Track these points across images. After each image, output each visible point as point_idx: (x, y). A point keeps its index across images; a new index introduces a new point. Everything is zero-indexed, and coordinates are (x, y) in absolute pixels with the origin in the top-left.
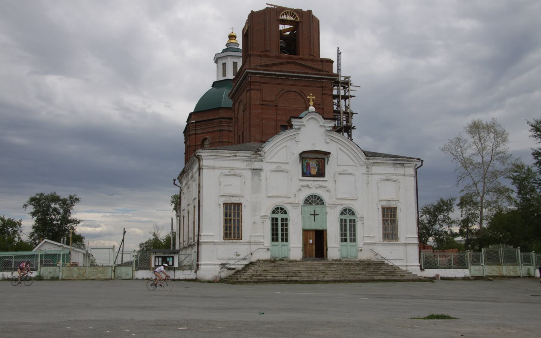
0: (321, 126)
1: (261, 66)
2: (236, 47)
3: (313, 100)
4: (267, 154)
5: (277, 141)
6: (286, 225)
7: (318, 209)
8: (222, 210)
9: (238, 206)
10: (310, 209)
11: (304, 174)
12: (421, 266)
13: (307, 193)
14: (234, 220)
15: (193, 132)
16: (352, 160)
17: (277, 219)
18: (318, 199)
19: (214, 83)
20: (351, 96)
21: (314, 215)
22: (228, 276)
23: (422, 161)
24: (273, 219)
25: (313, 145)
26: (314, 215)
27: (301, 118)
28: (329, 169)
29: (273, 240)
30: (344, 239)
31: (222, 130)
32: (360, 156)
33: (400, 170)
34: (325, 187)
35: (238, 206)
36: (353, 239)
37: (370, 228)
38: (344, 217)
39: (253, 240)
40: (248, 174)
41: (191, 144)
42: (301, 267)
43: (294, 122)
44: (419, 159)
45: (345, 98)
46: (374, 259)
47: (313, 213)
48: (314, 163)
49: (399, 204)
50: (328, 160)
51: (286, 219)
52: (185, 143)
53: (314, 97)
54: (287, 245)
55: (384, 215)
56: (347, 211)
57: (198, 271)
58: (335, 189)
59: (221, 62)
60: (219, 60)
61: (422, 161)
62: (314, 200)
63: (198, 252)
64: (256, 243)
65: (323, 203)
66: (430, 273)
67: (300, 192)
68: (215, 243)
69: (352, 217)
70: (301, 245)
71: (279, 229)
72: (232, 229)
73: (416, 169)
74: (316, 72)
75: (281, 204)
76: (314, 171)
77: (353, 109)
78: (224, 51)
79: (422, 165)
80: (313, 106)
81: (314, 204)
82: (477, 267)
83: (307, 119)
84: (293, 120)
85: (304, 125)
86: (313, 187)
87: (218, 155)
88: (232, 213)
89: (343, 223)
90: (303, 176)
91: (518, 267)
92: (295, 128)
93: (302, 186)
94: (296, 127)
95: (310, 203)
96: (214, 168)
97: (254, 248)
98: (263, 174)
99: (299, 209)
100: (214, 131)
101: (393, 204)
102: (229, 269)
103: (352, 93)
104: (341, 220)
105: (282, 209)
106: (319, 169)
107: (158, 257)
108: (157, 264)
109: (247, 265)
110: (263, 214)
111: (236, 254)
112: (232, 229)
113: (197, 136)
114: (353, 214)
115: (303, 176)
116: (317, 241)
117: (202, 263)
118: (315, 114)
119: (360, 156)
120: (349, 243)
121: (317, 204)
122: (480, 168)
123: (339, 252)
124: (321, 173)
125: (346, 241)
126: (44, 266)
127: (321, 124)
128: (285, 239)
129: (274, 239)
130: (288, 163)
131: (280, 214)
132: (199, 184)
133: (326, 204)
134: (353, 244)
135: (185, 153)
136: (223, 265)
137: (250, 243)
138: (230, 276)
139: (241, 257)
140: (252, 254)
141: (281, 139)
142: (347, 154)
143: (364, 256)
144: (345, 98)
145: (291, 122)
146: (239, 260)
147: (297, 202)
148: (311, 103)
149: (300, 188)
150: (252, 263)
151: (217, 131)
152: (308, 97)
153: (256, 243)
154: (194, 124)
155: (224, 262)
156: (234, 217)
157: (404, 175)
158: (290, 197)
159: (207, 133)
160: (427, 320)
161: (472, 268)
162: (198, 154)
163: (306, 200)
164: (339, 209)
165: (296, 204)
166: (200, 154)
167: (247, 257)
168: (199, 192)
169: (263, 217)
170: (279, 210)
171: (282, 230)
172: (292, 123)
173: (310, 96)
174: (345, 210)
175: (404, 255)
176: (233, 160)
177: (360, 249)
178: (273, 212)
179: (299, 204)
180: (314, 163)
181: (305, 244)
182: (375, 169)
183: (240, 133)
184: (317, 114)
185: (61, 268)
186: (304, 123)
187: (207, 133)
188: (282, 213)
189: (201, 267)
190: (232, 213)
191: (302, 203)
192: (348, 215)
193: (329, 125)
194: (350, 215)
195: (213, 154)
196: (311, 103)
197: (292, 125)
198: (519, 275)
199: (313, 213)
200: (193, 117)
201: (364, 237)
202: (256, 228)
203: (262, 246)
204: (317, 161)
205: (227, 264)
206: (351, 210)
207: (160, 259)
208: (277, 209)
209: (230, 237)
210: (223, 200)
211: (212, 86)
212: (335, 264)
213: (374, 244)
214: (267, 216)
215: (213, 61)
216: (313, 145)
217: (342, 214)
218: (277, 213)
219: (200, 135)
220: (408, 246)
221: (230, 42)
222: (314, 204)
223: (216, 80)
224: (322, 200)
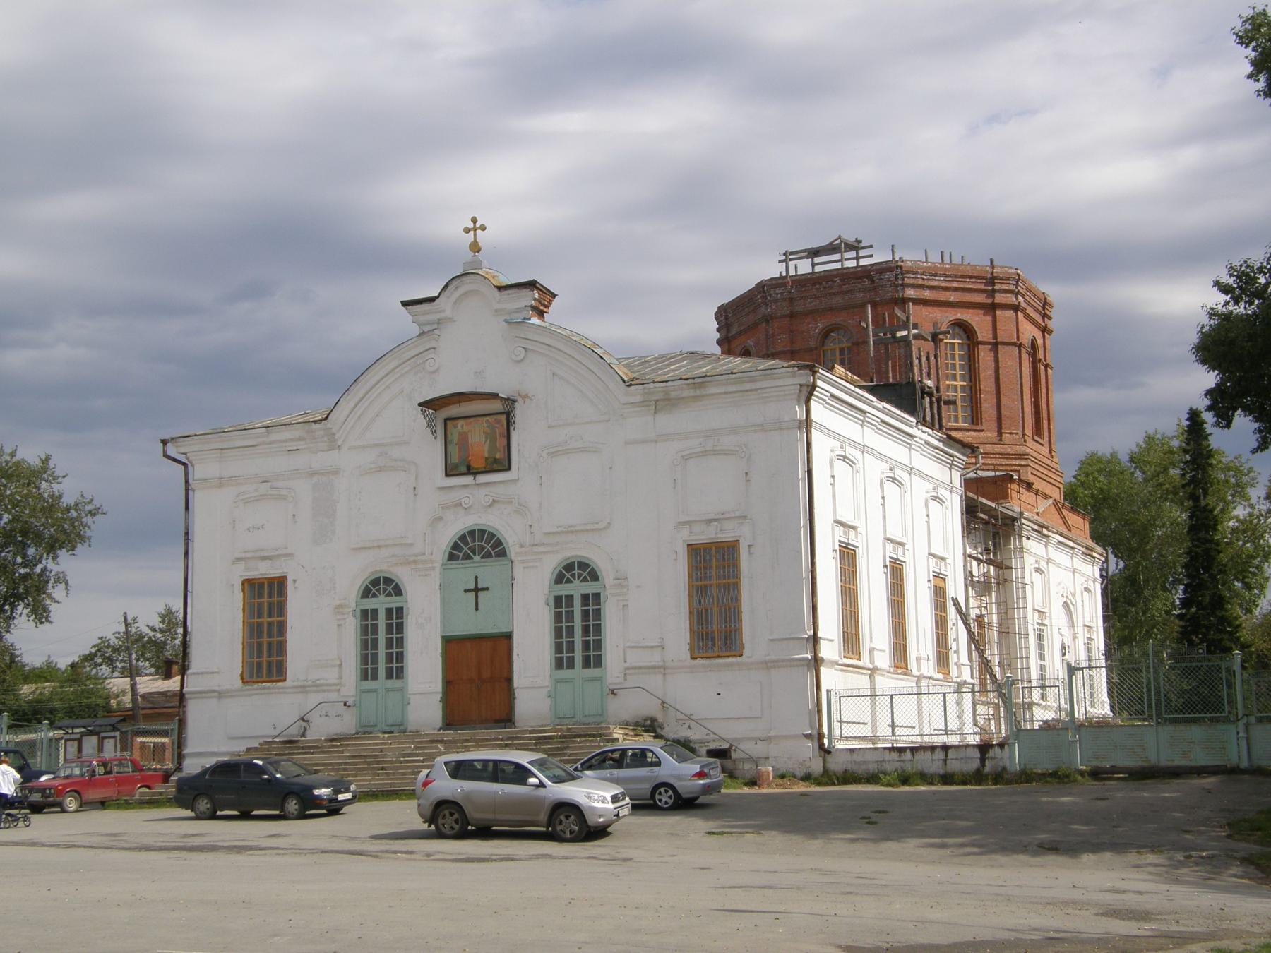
5: (377, 378)
6: (400, 628)
7: (487, 571)
9: (277, 586)
10: (465, 573)
14: (270, 624)
21: (477, 590)
28: (526, 440)
29: (364, 676)
30: (562, 661)
35: (277, 586)
36: (593, 658)
51: (400, 610)
54: (401, 689)
65: (503, 554)
68: (221, 695)
70: (438, 686)
72: (265, 657)
75: (384, 567)
81: (477, 558)
83: (454, 298)
86: (477, 504)
91: (1232, 728)
93: (444, 508)
95: (467, 557)
96: (221, 482)
99: (435, 577)
101: (264, 570)
104: (558, 600)
105: (388, 581)
114: (594, 576)
116: (479, 675)
120: (382, 682)
121: (488, 555)
123: (548, 702)
127: (497, 306)
128: (396, 670)
129: (367, 674)
131: (382, 598)
133: (513, 551)
134: (592, 672)
137: (303, 689)
141: (382, 374)
156: (270, 616)
158: (411, 545)
160: (1104, 919)
163: (456, 546)
164: (550, 564)
170: (382, 585)
174: (569, 567)
178: (366, 593)
186: (448, 313)
192: (577, 582)
193: (522, 304)
198: (1234, 761)
199: (480, 586)
206: (587, 565)
208: (375, 582)
210: (688, 536)
212: (441, 741)
217: (560, 579)
222: (477, 558)
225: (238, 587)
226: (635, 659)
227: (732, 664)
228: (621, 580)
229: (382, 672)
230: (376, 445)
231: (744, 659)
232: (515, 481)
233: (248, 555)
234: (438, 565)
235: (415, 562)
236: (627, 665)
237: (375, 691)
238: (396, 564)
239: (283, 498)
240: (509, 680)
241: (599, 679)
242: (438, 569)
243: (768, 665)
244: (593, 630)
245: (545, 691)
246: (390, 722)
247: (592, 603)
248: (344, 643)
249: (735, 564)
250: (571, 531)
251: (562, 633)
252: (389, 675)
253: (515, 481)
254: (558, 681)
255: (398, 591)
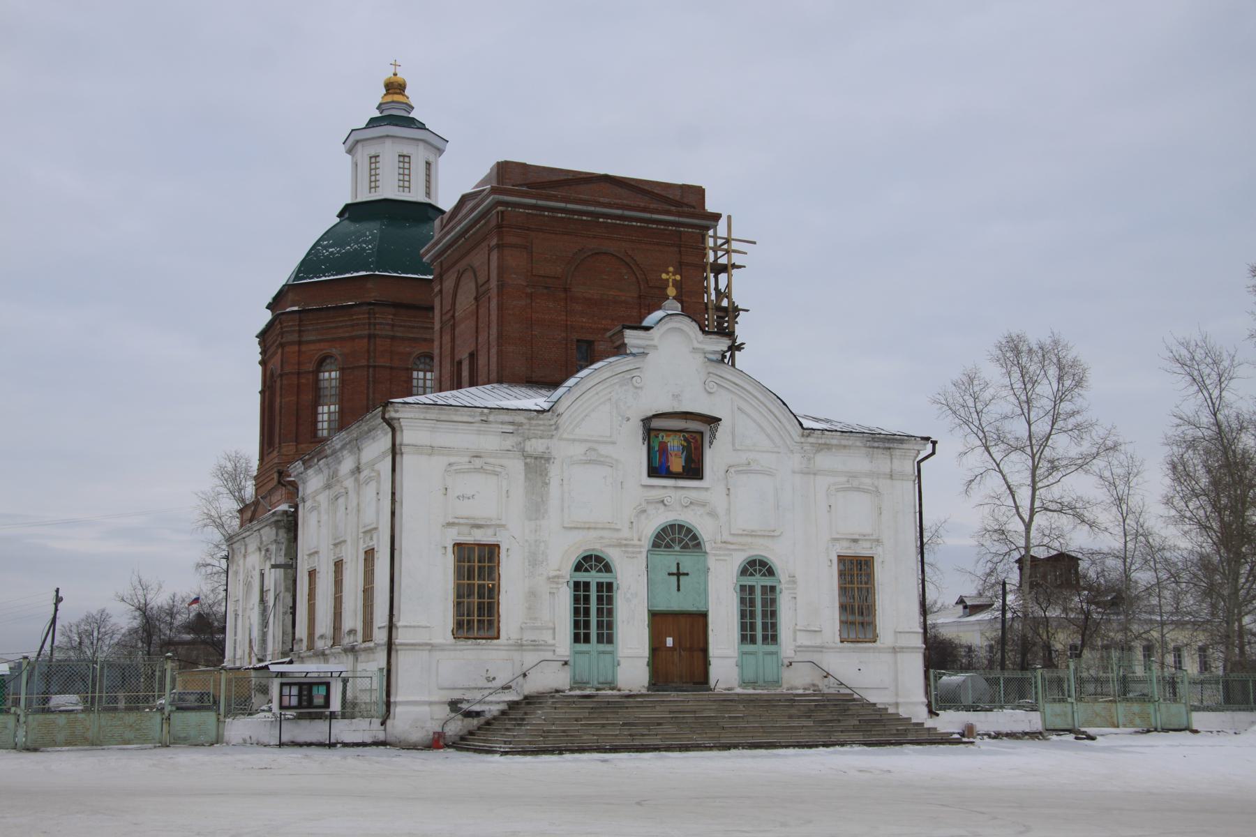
0: (695, 350)
1: (529, 186)
2: (406, 114)
3: (675, 283)
4: (565, 417)
7: (688, 562)
8: (450, 559)
9: (490, 553)
10: (668, 560)
11: (654, 472)
12: (929, 705)
13: (658, 520)
15: (295, 337)
16: (768, 436)
17: (587, 585)
18: (686, 536)
19: (348, 207)
20: (734, 266)
21: (678, 574)
22: (465, 732)
23: (934, 443)
24: (577, 584)
25: (676, 397)
26: (678, 574)
27: (647, 329)
28: (713, 459)
29: (577, 639)
30: (747, 635)
31: (375, 336)
32: (789, 427)
33: (882, 463)
34: (704, 505)
36: (771, 636)
37: (809, 607)
38: (748, 581)
39: (528, 636)
40: (516, 466)
41: (287, 370)
42: (658, 708)
43: (632, 338)
44: (927, 439)
45: (724, 269)
46: (828, 687)
47: (675, 571)
48: (677, 448)
49: (880, 549)
50: (713, 436)
51: (610, 586)
52: (263, 363)
53: (678, 277)
54: (611, 653)
55: (842, 574)
56: (757, 566)
57: (389, 722)
58: (729, 511)
59: (364, 153)
60: (359, 146)
61: (934, 443)
62: (677, 538)
63: (389, 671)
64: (536, 646)
65: (698, 545)
66: (949, 721)
67: (643, 517)
68: (432, 647)
69: (768, 581)
70: (645, 651)
71: (592, 608)
72: (477, 612)
73: (919, 463)
74: (667, 207)
75: (598, 547)
76: (677, 464)
77: (739, 299)
78: (373, 122)
79: (933, 453)
80: (674, 298)
82: (1058, 707)
84: (628, 332)
85: (655, 347)
86: (677, 502)
87: (443, 417)
88: (477, 570)
89: (746, 594)
90: (650, 475)
92: (634, 355)
93: (648, 502)
94: (634, 351)
95: (668, 546)
96: (432, 450)
97: (530, 658)
98: (554, 471)
100: (353, 338)
101: (862, 550)
102: (469, 714)
103: (736, 259)
106: (689, 460)
107: (290, 684)
108: (286, 702)
109: (513, 705)
110: (553, 573)
111: (486, 671)
112: (477, 612)
113: (304, 348)
114: (771, 572)
115: (650, 475)
116: (680, 641)
117: (399, 699)
118: (680, 318)
119: (789, 427)
120: (759, 647)
121: (685, 547)
122: (1022, 449)
124: (694, 470)
125: (587, 639)
126: (36, 712)
128: (607, 636)
129: (580, 636)
130: (614, 443)
132: (393, 494)
133: (708, 547)
134: (771, 648)
135: (262, 392)
136: (454, 705)
137: (520, 646)
138: (471, 733)
139: (499, 683)
140: (525, 675)
142: (755, 421)
143: (797, 680)
144: (724, 269)
145: (623, 337)
146: (496, 691)
147: (635, 542)
148: (671, 291)
149: (644, 504)
150: (530, 701)
151: (361, 337)
152: (664, 276)
153: (534, 643)
154: (297, 316)
155: (456, 695)
157: (891, 476)
158: (618, 530)
159: (334, 340)
161: (1049, 708)
162: (393, 415)
163: (658, 536)
164: (739, 559)
165: (634, 546)
166: (396, 415)
167: (513, 684)
168: (393, 514)
169: (553, 579)
170: (590, 562)
171: (587, 612)
172: (626, 341)
173: (667, 273)
175: (890, 676)
176: (479, 432)
177: (786, 662)
178: (578, 568)
179: (641, 546)
180: (677, 448)
181: (656, 649)
182: (824, 460)
183: (464, 355)
184: (687, 320)
185: (22, 719)
186: (655, 342)
187: (334, 340)
188: (600, 571)
189: (398, 711)
190: (477, 570)
191: (646, 543)
192: (758, 576)
194: (764, 575)
195: (428, 416)
196: (671, 291)
197: (624, 345)
199: (675, 571)
200: (290, 296)
201: (795, 632)
202: (534, 602)
203: (549, 655)
204: (686, 440)
205: (461, 701)
207: (295, 691)
208: (587, 558)
209: (470, 628)
210: (453, 536)
211: (340, 215)
213: (820, 649)
214: (563, 577)
215: (343, 149)
216: (676, 397)
217: (744, 572)
218: (586, 570)
219: (312, 347)
220: (899, 655)
221: (389, 98)
222: (677, 548)
223: (349, 201)
224: (695, 537)
225: (450, 550)
226: (803, 640)
227: (870, 648)
228: (793, 579)
229: (593, 637)
230: (586, 441)
231: (878, 644)
232: (707, 489)
233: (461, 521)
234: (644, 550)
235: (626, 545)
236: (799, 643)
237: (588, 653)
238: (610, 546)
239: (496, 474)
240: (705, 650)
241: (776, 653)
242: (644, 555)
243: (895, 650)
244: (771, 614)
245: (734, 660)
246: (601, 680)
247: (770, 592)
248: (560, 610)
249: (870, 576)
250: (752, 534)
251: (746, 615)
252: (600, 640)
253: (707, 489)
254: (744, 653)
255: (607, 568)
